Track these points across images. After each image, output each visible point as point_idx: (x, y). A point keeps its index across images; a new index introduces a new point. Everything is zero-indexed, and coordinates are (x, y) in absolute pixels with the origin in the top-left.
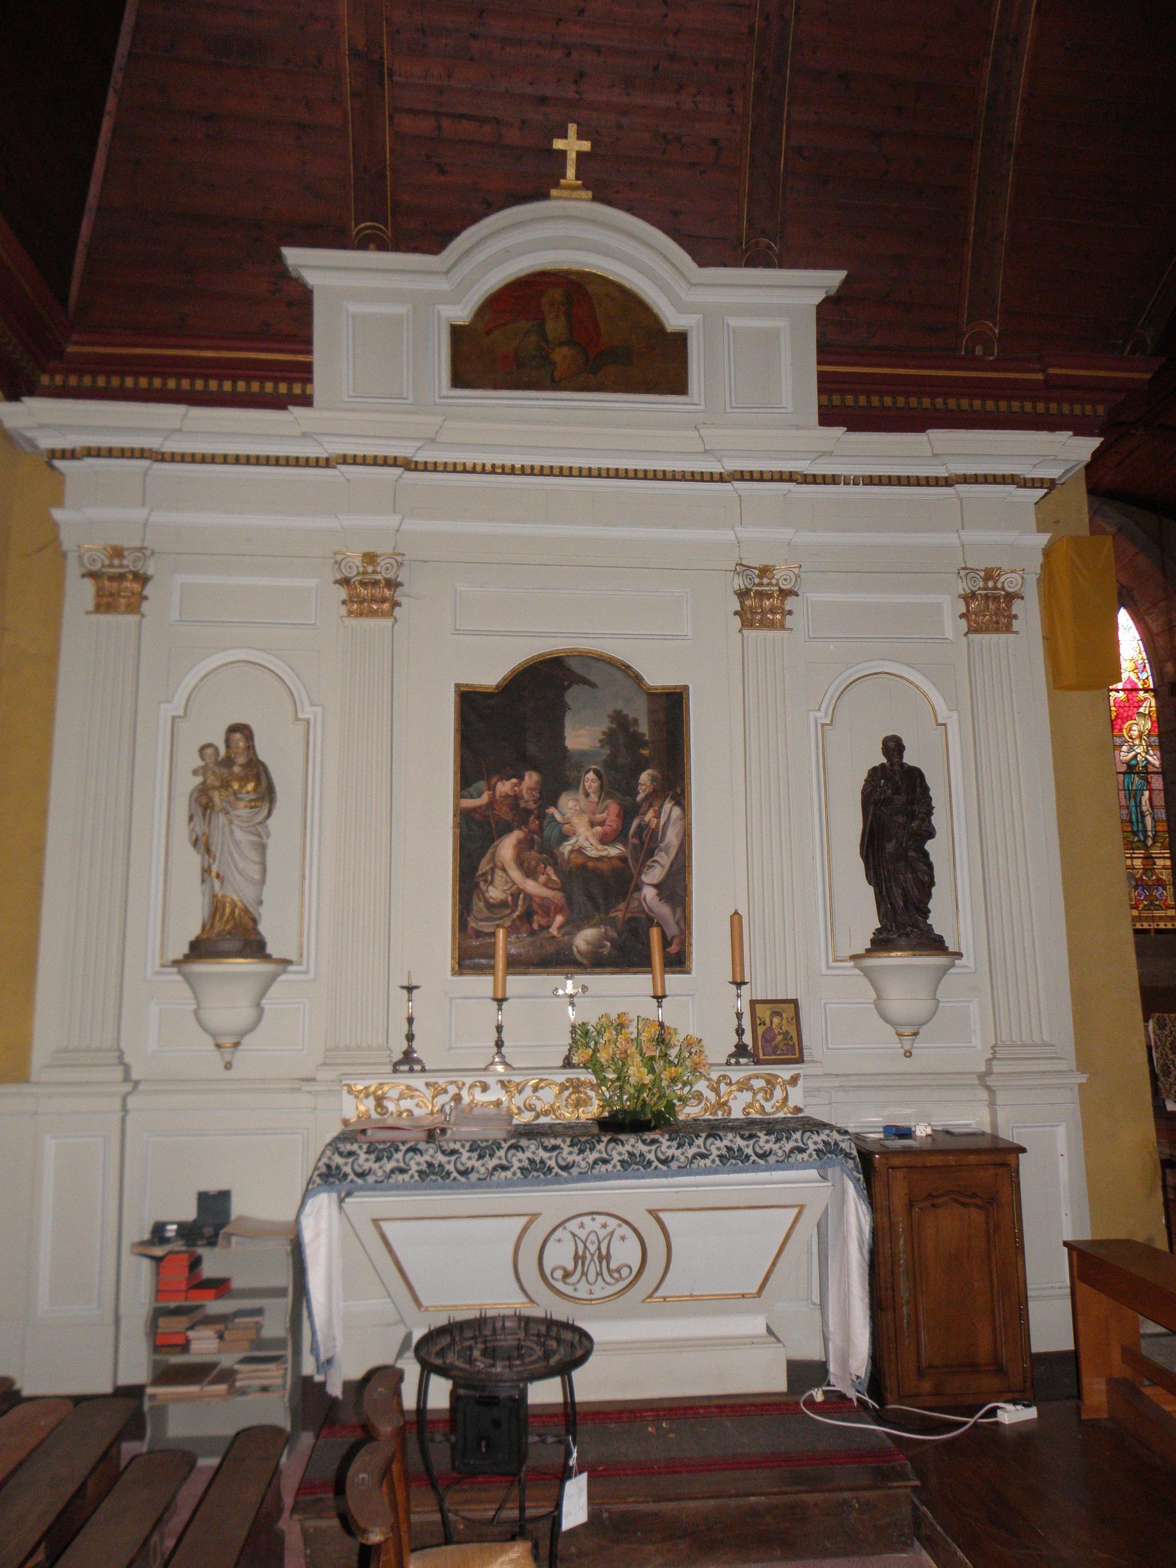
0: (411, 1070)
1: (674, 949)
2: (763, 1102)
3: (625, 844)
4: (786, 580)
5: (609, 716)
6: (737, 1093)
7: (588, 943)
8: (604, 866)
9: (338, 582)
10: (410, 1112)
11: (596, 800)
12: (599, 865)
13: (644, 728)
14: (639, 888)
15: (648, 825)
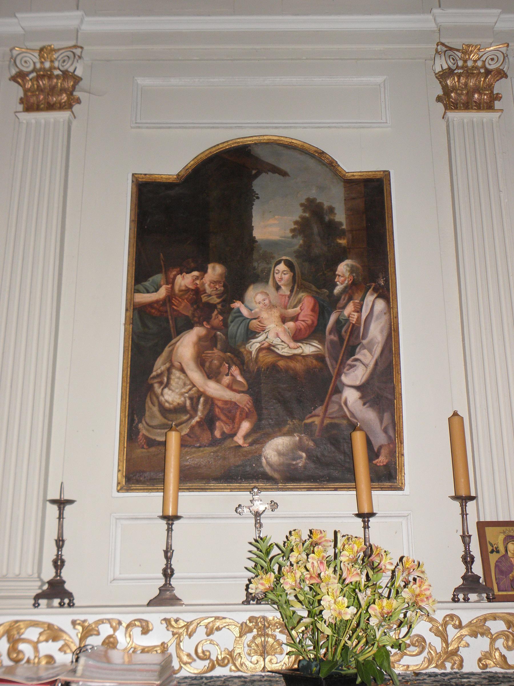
0: (61, 605)
1: (382, 460)
2: (504, 652)
3: (322, 341)
4: (492, 59)
5: (302, 205)
6: (468, 639)
7: (280, 454)
8: (298, 366)
9: (14, 79)
10: (50, 658)
11: (288, 293)
12: (292, 364)
13: (340, 216)
14: (338, 391)
15: (347, 320)
